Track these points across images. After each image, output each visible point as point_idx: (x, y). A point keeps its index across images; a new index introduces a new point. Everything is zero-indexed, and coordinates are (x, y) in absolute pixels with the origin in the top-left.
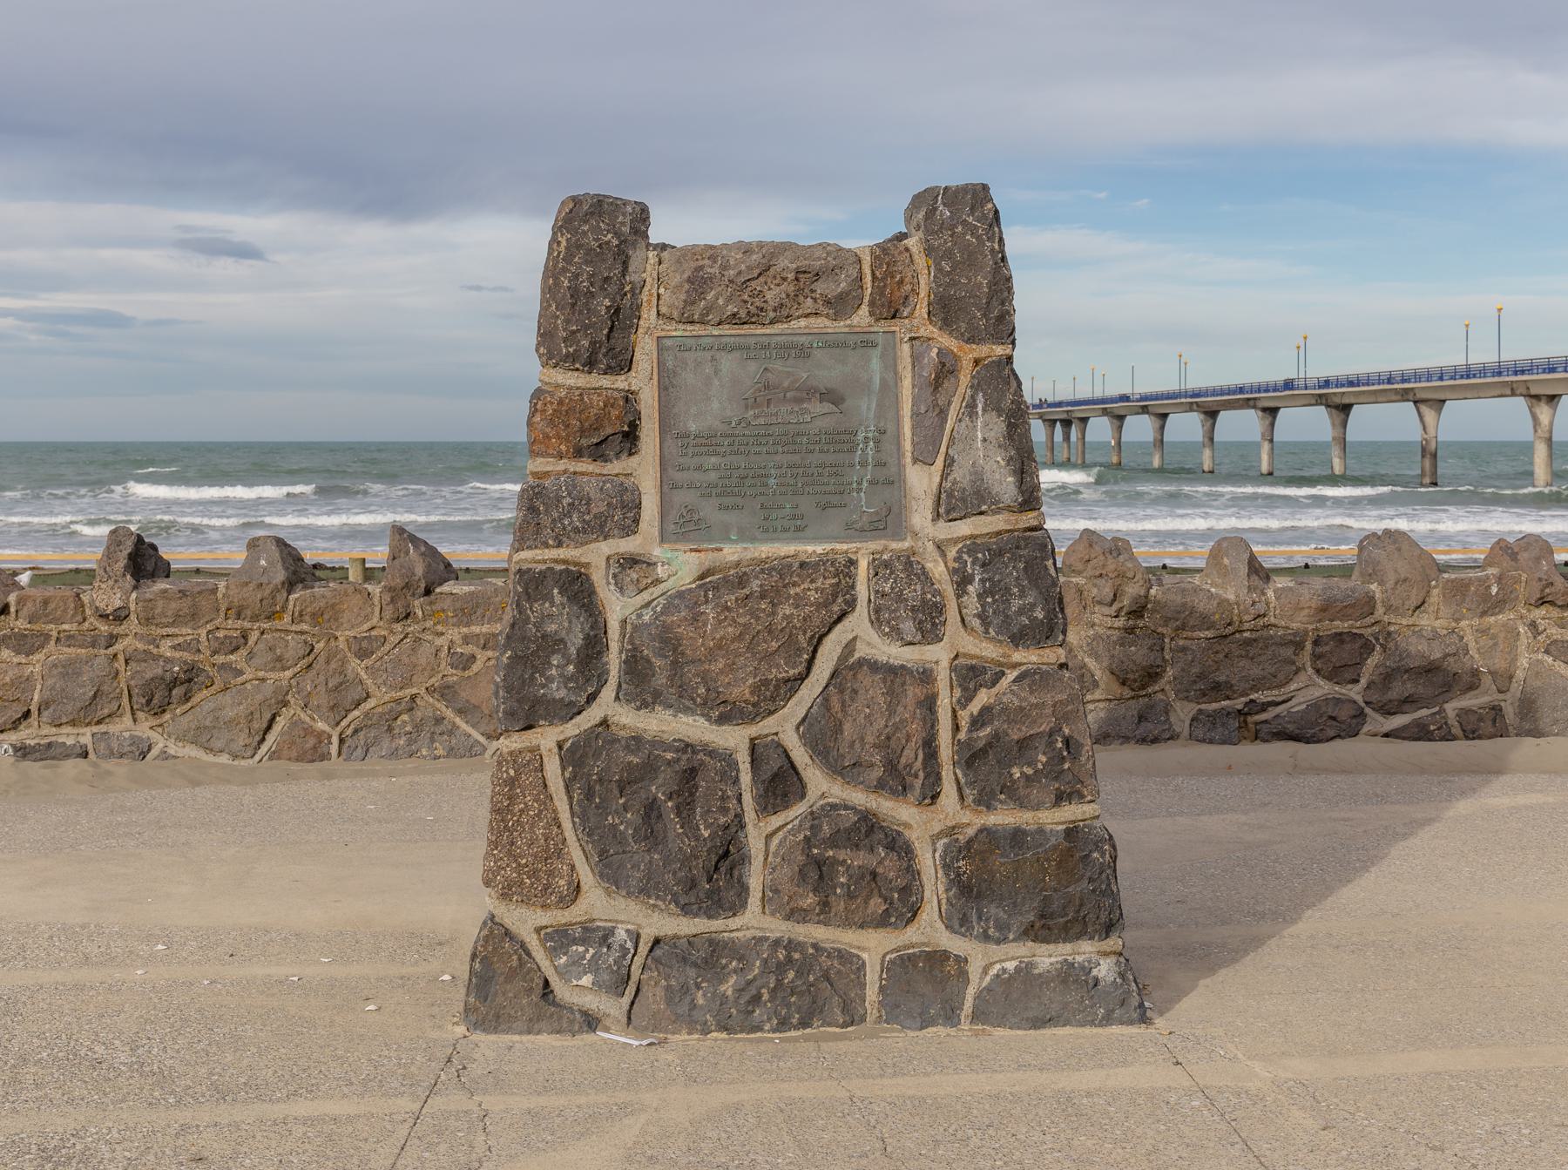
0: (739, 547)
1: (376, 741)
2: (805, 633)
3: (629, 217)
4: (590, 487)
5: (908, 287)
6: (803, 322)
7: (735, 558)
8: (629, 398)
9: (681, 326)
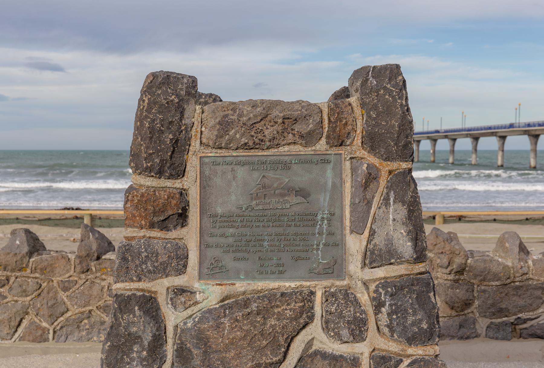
0: (245, 283)
1: (72, 333)
2: (283, 335)
3: (185, 86)
4: (158, 246)
5: (350, 127)
6: (286, 148)
7: (242, 289)
8: (183, 193)
9: (214, 150)
